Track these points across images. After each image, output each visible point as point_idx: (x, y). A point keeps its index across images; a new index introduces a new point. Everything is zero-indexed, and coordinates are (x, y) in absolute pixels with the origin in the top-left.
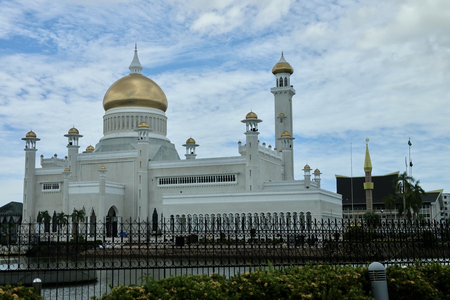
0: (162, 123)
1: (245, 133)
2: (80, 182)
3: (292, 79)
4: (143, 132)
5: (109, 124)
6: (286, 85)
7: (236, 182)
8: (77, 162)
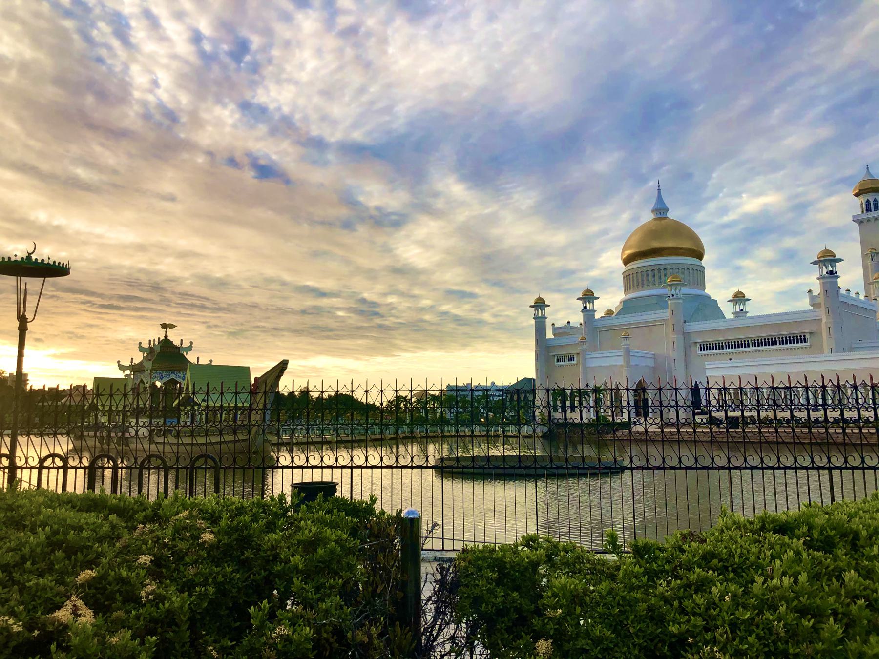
5: (631, 281)
7: (808, 344)
8: (594, 329)
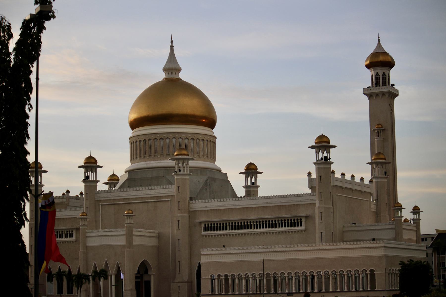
0: (209, 145)
1: (314, 163)
2: (101, 230)
3: (395, 75)
4: (181, 163)
5: (138, 149)
6: (384, 84)
7: (303, 228)
